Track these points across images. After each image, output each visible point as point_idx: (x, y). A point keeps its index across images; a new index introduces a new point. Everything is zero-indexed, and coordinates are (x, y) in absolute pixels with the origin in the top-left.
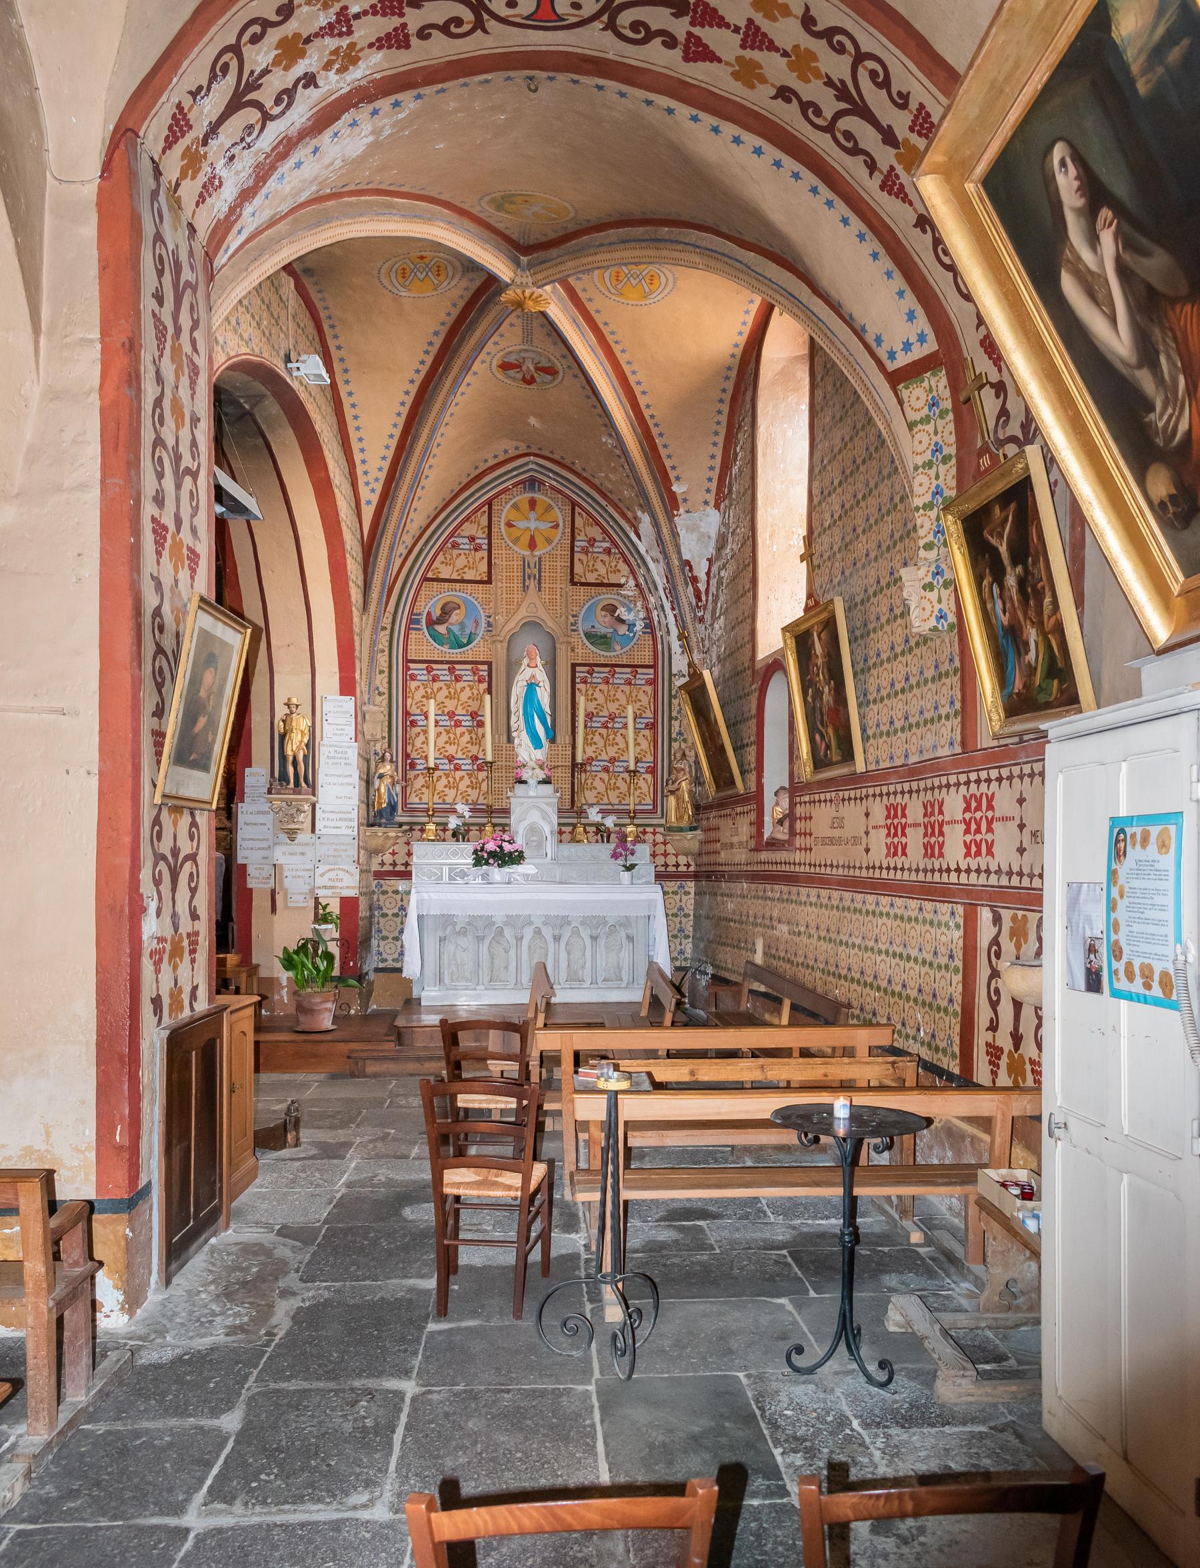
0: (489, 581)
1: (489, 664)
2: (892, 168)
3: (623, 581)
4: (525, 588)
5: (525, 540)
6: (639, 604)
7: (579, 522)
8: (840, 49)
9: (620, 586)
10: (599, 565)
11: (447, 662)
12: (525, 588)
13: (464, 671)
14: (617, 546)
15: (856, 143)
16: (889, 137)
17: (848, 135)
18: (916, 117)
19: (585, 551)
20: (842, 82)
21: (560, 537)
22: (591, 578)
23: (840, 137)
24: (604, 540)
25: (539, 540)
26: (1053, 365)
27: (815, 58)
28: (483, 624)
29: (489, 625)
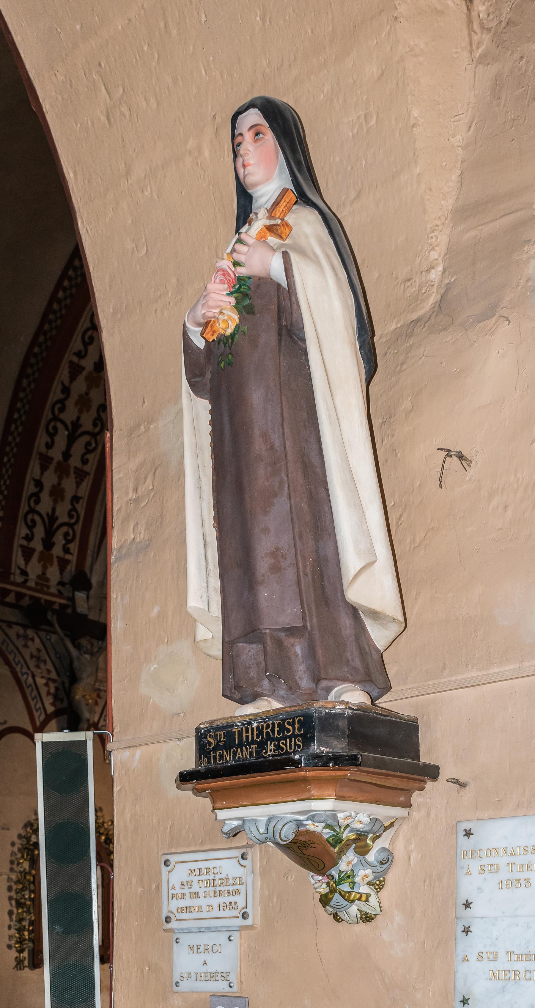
16: (67, 455)
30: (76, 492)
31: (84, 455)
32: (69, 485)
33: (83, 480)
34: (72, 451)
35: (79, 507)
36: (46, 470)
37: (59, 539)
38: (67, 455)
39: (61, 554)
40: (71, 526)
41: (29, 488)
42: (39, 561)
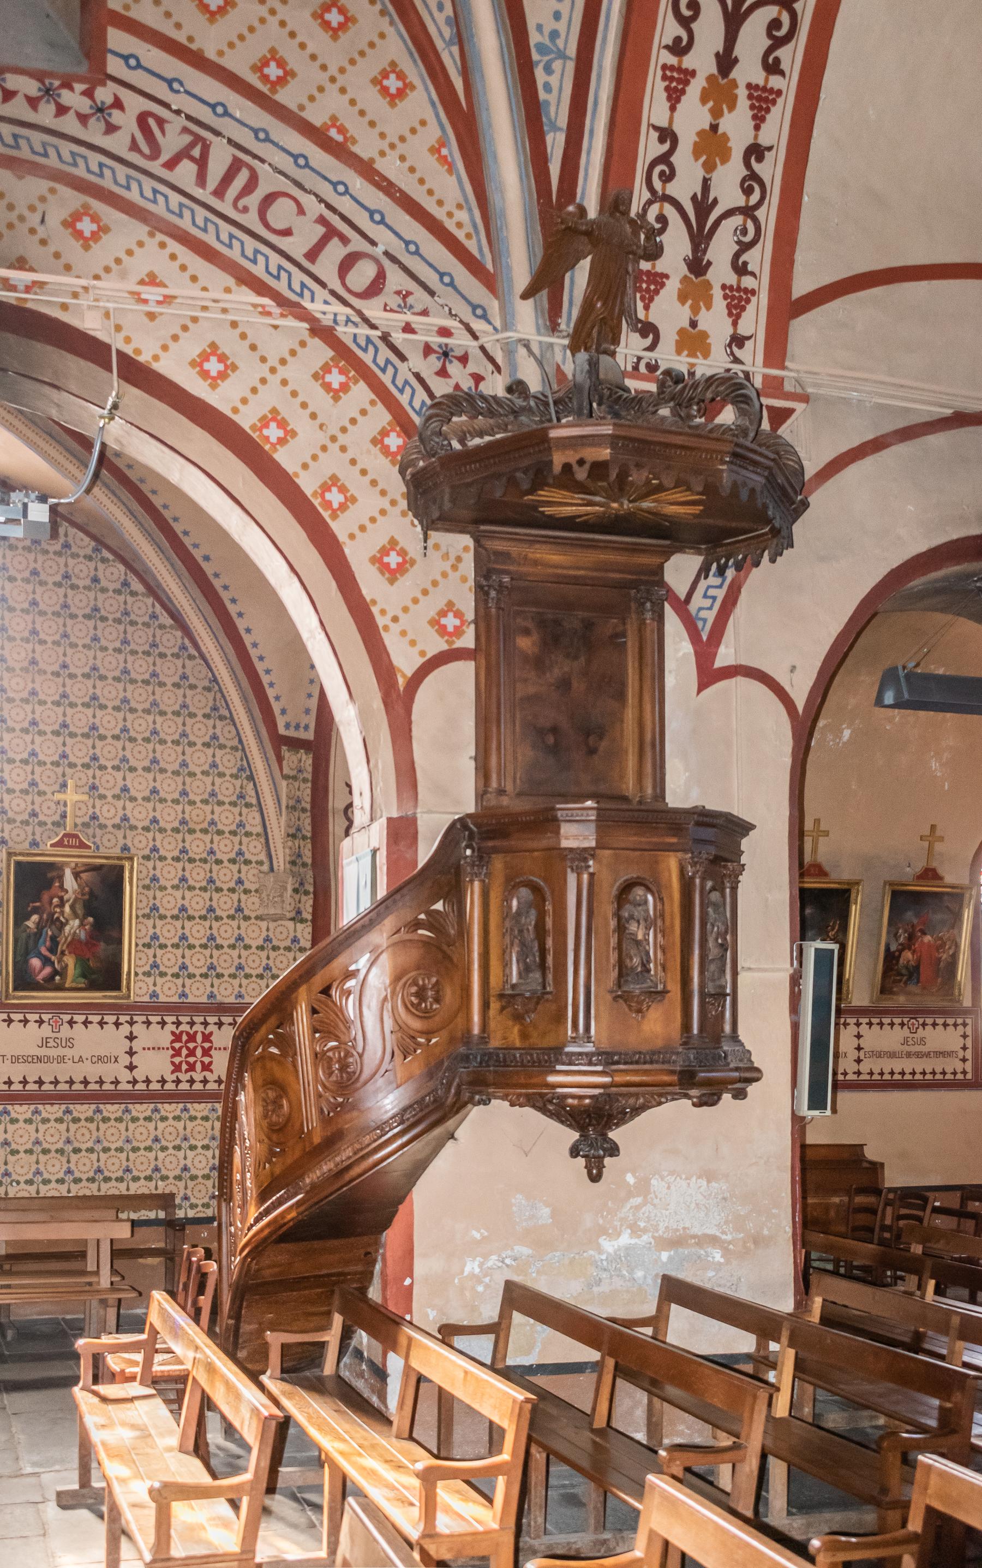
2: (693, 73)
16: (726, 61)
30: (756, 137)
31: (737, 256)
32: (737, 126)
33: (743, 309)
34: (738, 51)
35: (752, 258)
36: (678, 100)
37: (721, 249)
38: (726, 61)
39: (732, 279)
40: (748, 211)
41: (649, 147)
42: (704, 99)
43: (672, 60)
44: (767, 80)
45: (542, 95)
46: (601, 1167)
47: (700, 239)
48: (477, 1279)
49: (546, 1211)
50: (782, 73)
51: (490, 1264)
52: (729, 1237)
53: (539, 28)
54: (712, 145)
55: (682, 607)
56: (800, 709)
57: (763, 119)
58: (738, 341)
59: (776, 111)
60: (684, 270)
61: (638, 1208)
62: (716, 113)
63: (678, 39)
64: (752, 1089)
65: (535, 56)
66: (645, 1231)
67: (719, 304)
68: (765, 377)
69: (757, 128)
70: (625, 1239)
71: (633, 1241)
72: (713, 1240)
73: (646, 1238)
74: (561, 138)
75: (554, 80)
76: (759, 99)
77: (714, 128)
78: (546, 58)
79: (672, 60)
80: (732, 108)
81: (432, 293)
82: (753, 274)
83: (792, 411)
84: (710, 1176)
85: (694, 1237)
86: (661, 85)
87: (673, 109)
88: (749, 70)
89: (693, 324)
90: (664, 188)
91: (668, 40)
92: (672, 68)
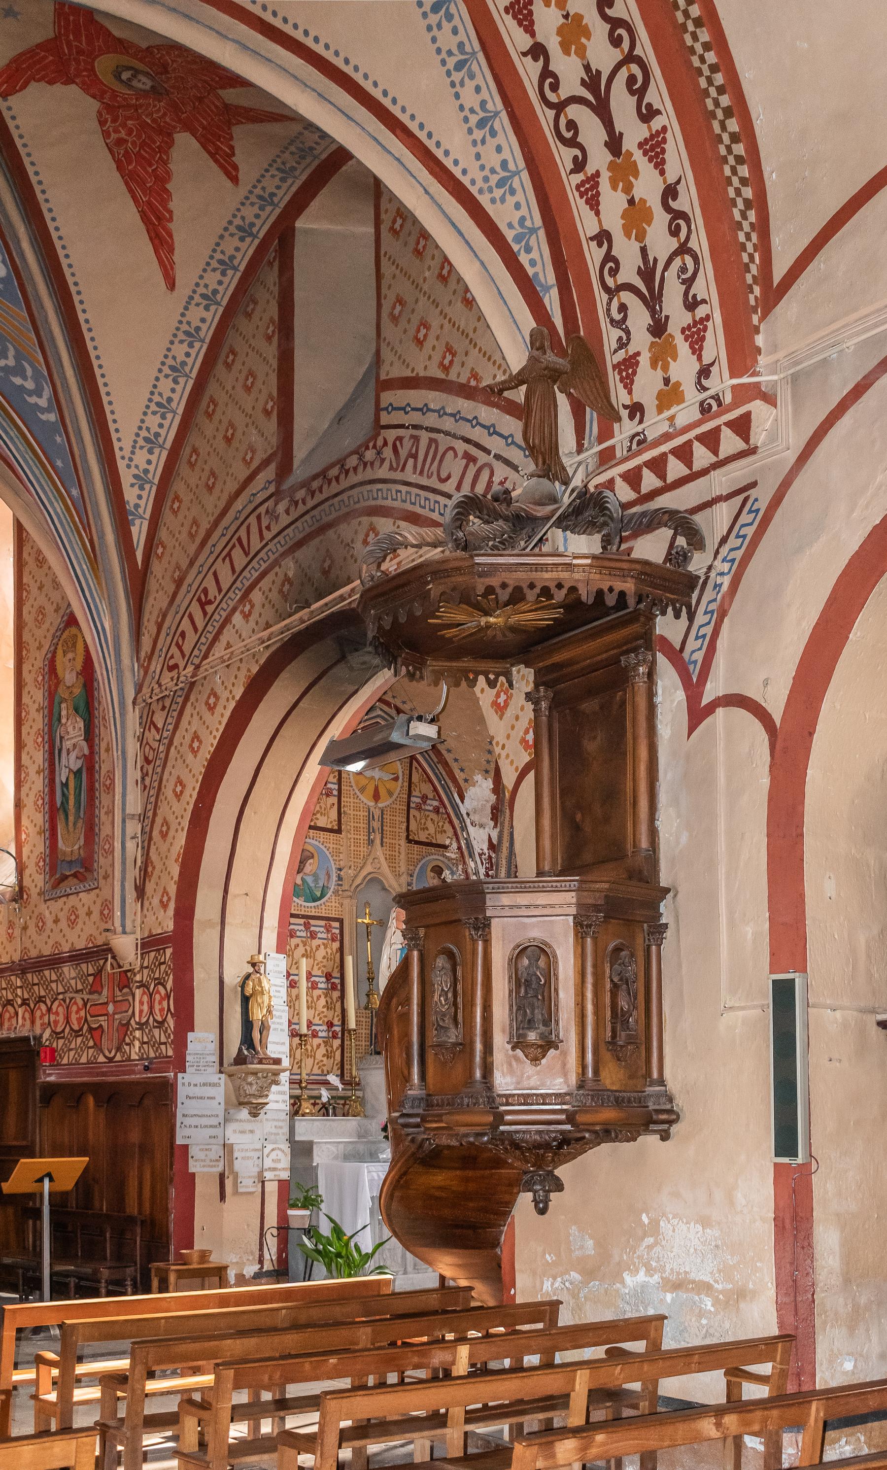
0: (339, 831)
1: (341, 921)
2: (598, 174)
3: (447, 842)
4: (371, 842)
5: (370, 790)
6: (460, 867)
7: (415, 778)
8: (616, 42)
9: (445, 847)
10: (429, 824)
11: (303, 917)
12: (371, 842)
13: (318, 926)
14: (445, 808)
15: (576, 134)
16: (614, 143)
17: (572, 125)
18: (652, 137)
19: (419, 808)
20: (599, 73)
21: (399, 787)
22: (423, 837)
23: (563, 122)
24: (434, 799)
25: (382, 792)
26: (34, 1236)
27: (588, 35)
28: (334, 878)
29: (340, 878)
33: (703, 339)
35: (699, 289)
42: (614, 188)
43: (580, 177)
44: (650, 128)
45: (530, 271)
46: (546, 1201)
47: (653, 300)
48: (701, 1314)
49: (590, 1243)
50: (658, 112)
51: (556, 1285)
52: (719, 1287)
53: (510, 226)
54: (636, 216)
55: (676, 656)
56: (777, 718)
57: (663, 162)
58: (705, 372)
59: (669, 146)
60: (649, 338)
61: (650, 1247)
62: (628, 189)
63: (575, 158)
64: (674, 1129)
65: (515, 247)
66: (655, 1270)
67: (683, 347)
68: (734, 388)
69: (662, 173)
70: (641, 1276)
71: (646, 1279)
72: (705, 1288)
73: (656, 1278)
74: (555, 292)
75: (535, 255)
76: (652, 149)
77: (631, 202)
78: (523, 243)
79: (580, 177)
80: (636, 174)
81: (515, 468)
82: (704, 301)
83: (748, 415)
84: (705, 1222)
85: (693, 1282)
86: (581, 202)
87: (597, 213)
88: (633, 134)
89: (667, 381)
90: (615, 281)
91: (570, 166)
92: (583, 183)
